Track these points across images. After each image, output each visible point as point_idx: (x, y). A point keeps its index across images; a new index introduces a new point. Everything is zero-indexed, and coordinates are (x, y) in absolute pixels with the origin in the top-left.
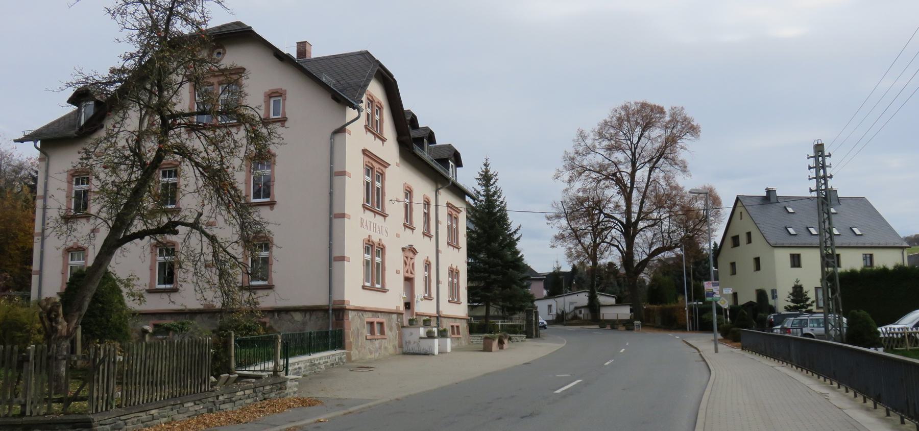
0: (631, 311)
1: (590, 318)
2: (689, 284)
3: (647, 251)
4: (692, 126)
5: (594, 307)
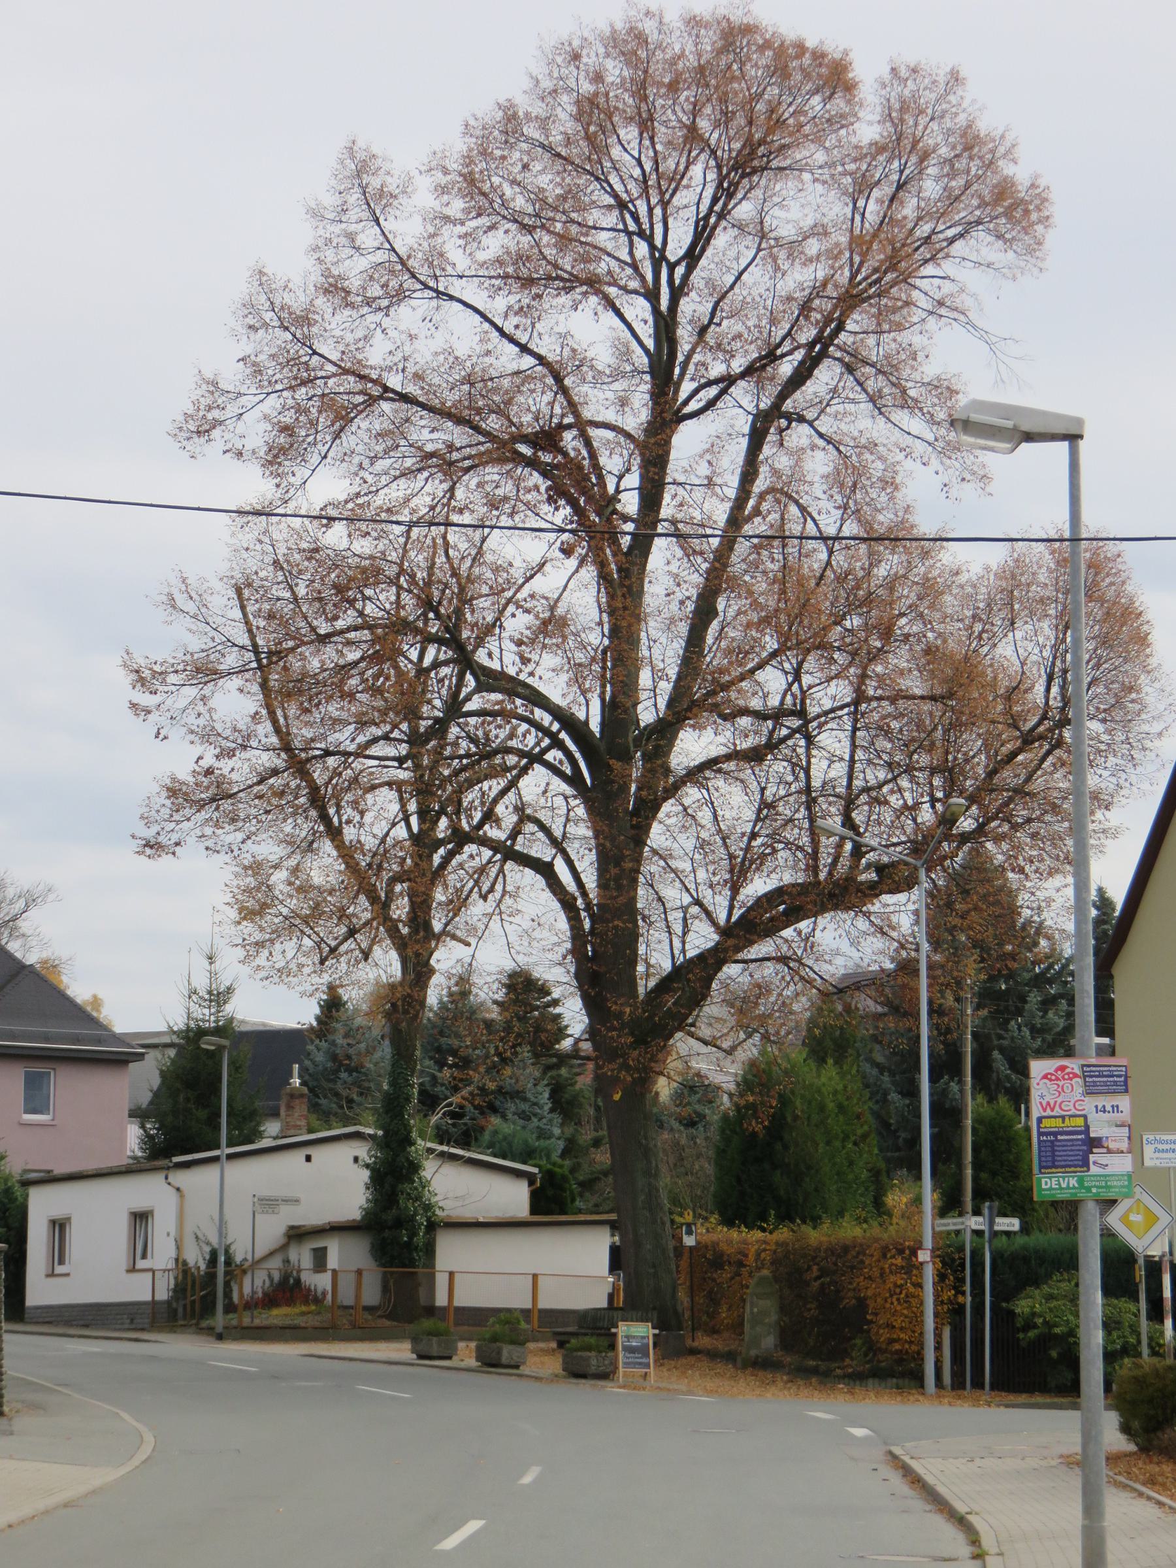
0: (617, 1260)
1: (372, 1294)
2: (947, 1114)
3: (720, 905)
4: (1004, 191)
5: (397, 1229)
